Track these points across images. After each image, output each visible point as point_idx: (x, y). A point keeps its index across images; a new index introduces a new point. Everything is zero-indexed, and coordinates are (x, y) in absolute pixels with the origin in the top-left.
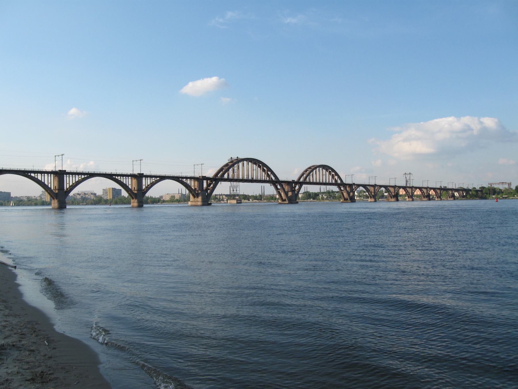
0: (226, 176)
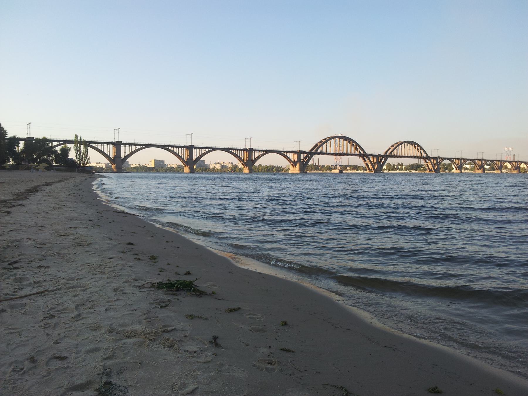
0: (319, 150)
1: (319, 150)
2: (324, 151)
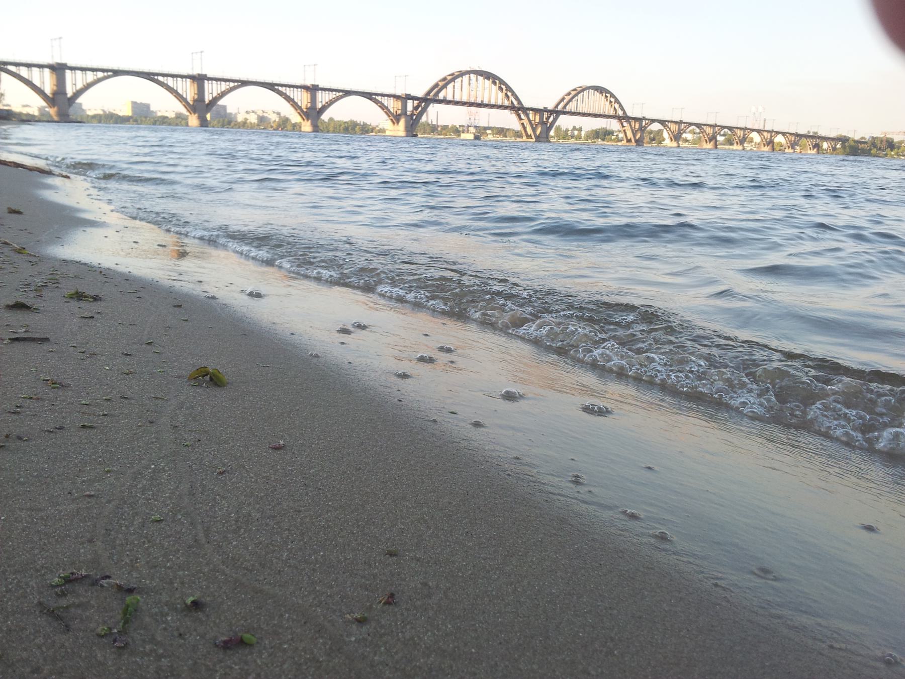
2: (449, 98)
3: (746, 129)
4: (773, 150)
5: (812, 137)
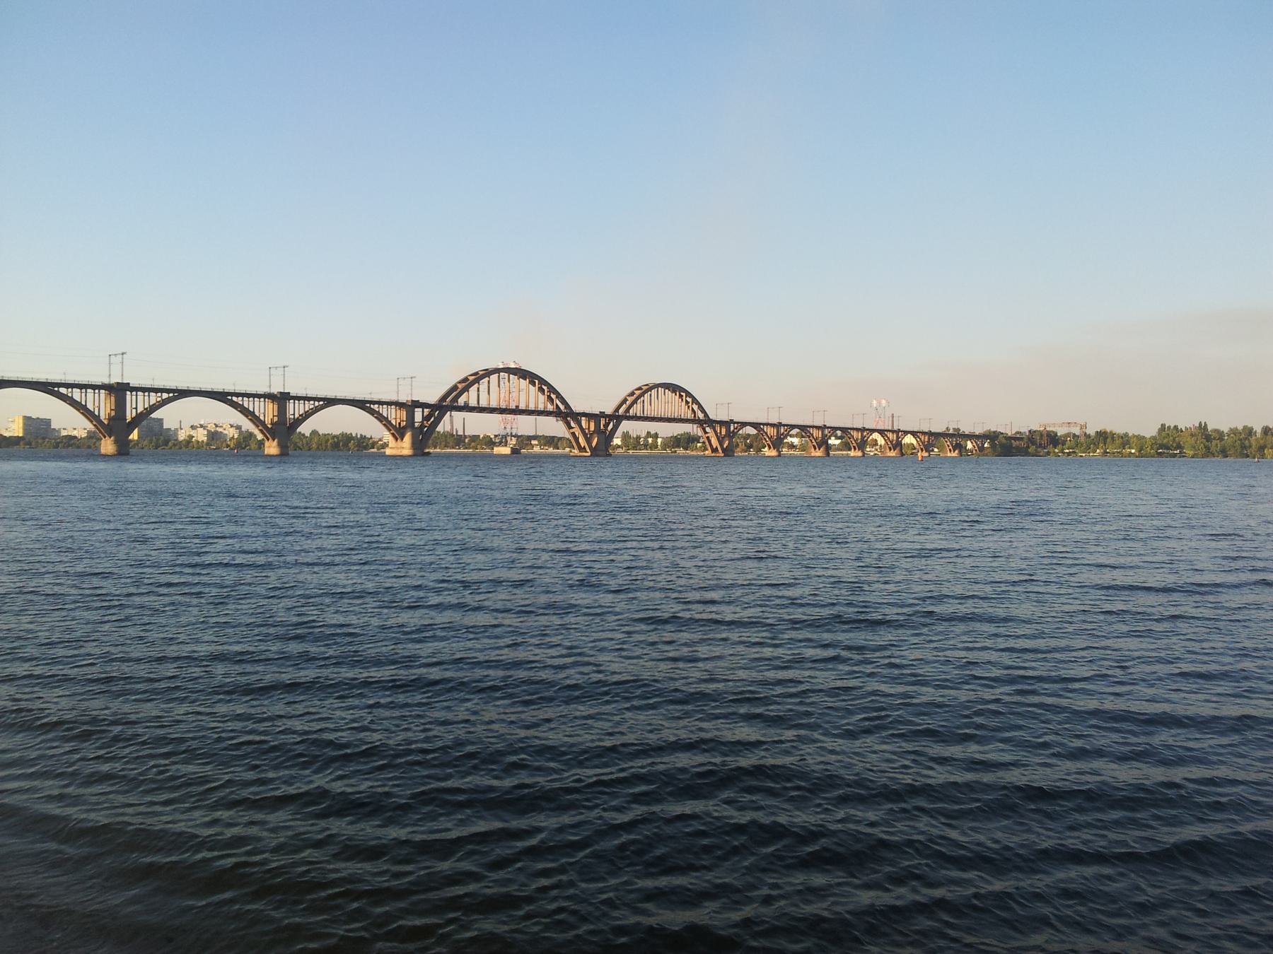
0: (461, 401)
1: (461, 401)
2: (473, 403)
3: (864, 429)
4: (902, 455)
5: (952, 436)
